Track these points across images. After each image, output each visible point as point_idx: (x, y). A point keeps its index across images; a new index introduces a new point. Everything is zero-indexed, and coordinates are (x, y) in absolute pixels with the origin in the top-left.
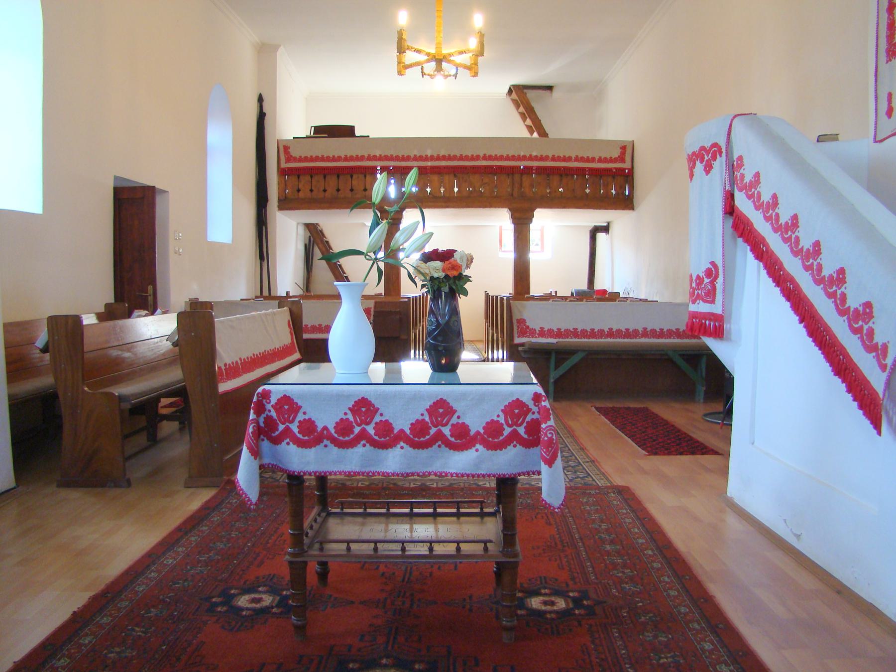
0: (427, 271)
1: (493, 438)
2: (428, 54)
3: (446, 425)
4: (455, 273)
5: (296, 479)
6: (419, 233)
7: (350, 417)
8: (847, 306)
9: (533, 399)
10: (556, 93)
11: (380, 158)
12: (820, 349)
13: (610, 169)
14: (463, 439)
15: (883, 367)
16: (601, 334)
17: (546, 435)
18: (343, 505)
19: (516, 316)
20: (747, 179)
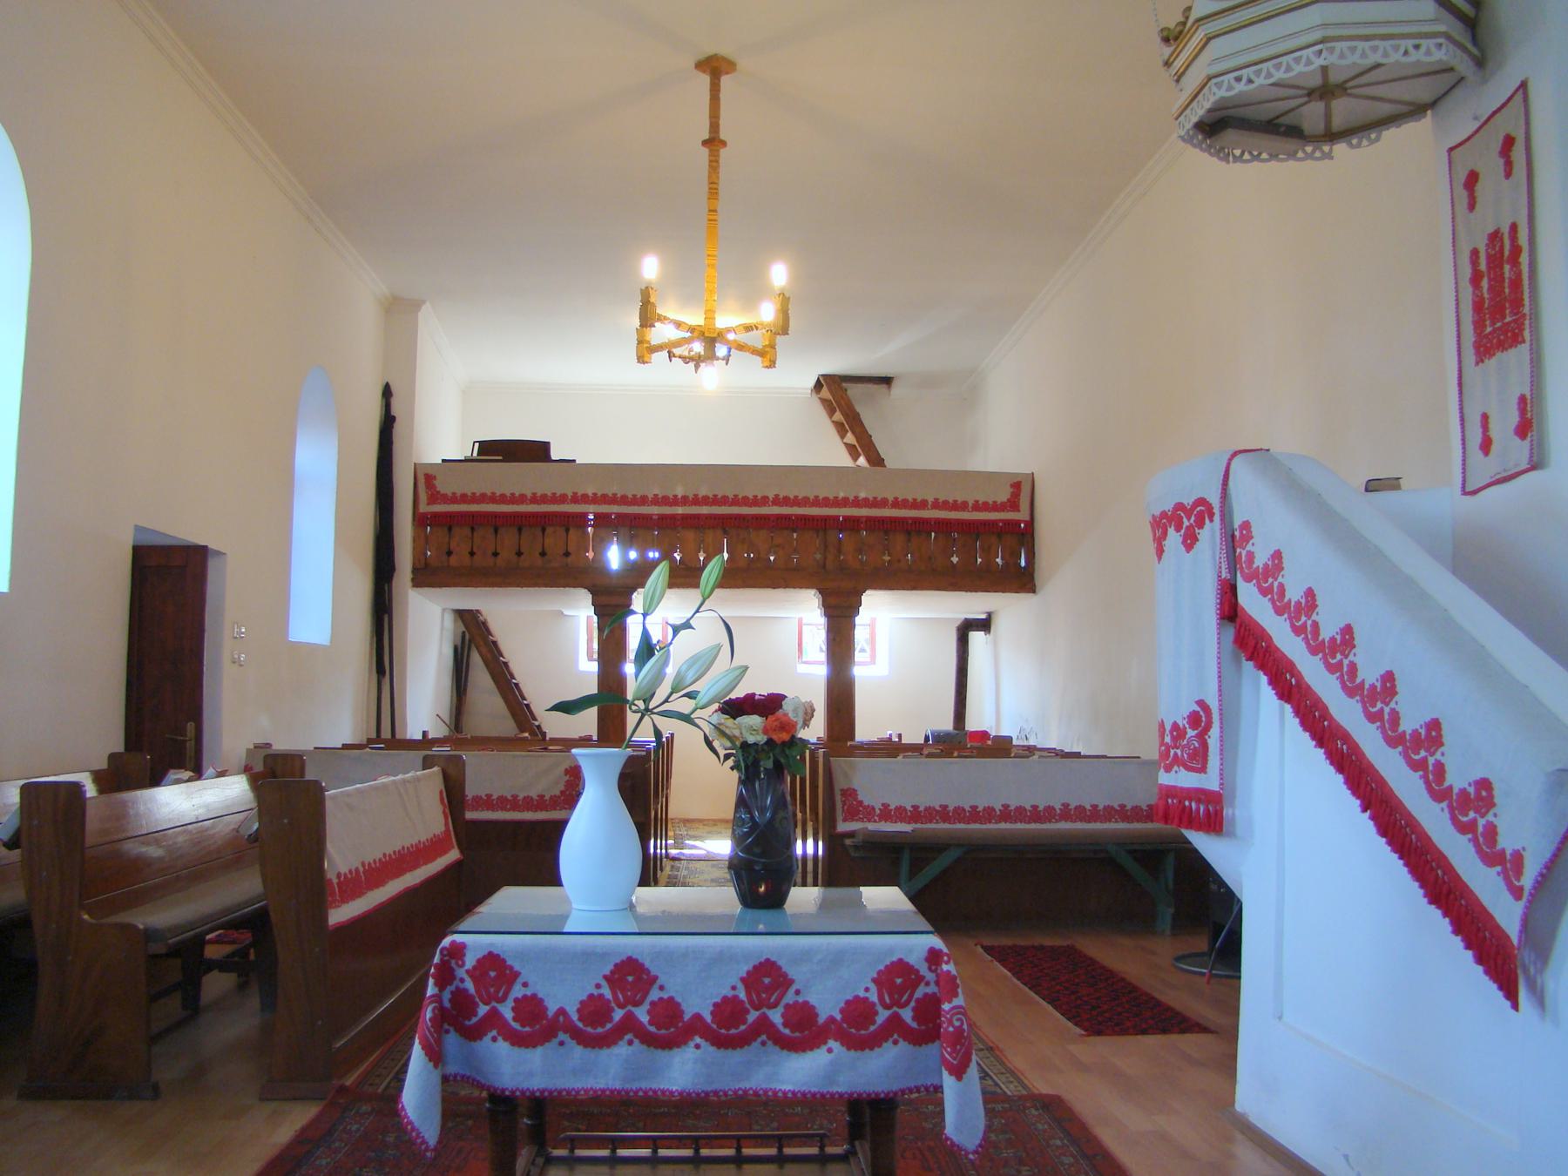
0: (736, 732)
1: (858, 1029)
2: (692, 329)
3: (775, 1005)
4: (785, 737)
5: (503, 1105)
6: (723, 663)
7: (606, 992)
8: (1446, 784)
9: (928, 960)
10: (896, 390)
11: (595, 500)
12: (1401, 858)
13: (993, 523)
14: (805, 1031)
15: (1517, 893)
16: (989, 814)
17: (950, 1022)
18: (573, 1143)
19: (840, 784)
20: (1260, 560)
